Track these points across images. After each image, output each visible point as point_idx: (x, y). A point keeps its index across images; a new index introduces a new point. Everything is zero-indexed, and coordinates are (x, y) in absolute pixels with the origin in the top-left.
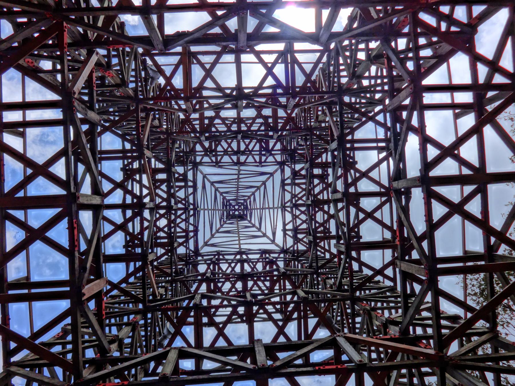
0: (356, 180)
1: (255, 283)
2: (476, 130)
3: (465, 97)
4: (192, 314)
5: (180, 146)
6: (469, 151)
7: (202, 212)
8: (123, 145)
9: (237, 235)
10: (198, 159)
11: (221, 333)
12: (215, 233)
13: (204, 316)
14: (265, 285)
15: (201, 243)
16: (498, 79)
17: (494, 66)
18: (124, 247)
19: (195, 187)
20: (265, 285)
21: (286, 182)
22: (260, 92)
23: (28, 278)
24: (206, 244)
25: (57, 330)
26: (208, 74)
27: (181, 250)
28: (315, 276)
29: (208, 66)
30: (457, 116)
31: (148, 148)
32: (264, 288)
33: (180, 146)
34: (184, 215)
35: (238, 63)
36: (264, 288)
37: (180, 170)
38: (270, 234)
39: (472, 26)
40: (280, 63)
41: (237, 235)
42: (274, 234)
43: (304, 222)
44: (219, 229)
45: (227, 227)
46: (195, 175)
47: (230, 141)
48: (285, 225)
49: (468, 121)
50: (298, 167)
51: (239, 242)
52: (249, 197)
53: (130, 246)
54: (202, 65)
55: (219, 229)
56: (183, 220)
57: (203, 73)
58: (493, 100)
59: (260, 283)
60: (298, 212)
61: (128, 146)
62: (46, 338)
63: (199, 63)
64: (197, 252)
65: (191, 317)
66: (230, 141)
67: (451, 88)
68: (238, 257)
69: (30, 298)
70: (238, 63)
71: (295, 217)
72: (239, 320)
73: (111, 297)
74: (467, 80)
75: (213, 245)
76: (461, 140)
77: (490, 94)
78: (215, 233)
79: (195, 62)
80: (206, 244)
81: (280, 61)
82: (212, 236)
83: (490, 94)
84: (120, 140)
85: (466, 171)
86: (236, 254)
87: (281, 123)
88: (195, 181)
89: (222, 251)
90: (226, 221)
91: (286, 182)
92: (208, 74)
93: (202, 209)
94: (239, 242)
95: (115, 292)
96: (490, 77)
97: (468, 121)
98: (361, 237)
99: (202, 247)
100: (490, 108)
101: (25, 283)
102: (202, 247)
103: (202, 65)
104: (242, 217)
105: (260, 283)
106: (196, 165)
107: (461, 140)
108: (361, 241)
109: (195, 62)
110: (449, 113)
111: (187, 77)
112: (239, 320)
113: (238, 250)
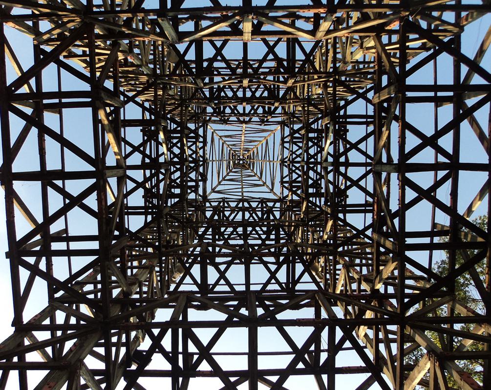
0: (146, 180)
1: (254, 229)
2: (49, 220)
3: (56, 246)
4: (297, 70)
5: (193, 107)
6: (56, 202)
7: (210, 163)
8: (345, 216)
9: (240, 183)
10: (278, 205)
11: (271, 49)
12: (222, 181)
13: (170, 352)
14: (262, 230)
15: (209, 190)
16: (31, 260)
17: (35, 271)
18: (348, 131)
19: (205, 142)
20: (262, 230)
21: (285, 140)
22: (230, 259)
23: (437, 106)
24: (213, 191)
25: (413, 62)
26: (273, 275)
27: (192, 196)
28: (158, 71)
29: (273, 281)
30: (66, 231)
31: (327, 213)
32: (260, 232)
33: (193, 107)
34: (293, 157)
35: (248, 283)
36: (260, 232)
37: (192, 126)
38: (269, 183)
39: (54, 304)
40: (211, 285)
41: (240, 183)
42: (273, 184)
43: (299, 176)
44: (225, 177)
45: (232, 175)
46: (205, 132)
47: (270, 287)
48: (282, 178)
49: (56, 227)
50: (296, 127)
51: (242, 190)
52: (231, 171)
53: (343, 131)
54: (278, 282)
55: (225, 177)
56: (294, 153)
57: (277, 275)
58: (36, 244)
59: (258, 229)
60: (194, 156)
61: (341, 216)
62: (424, 54)
63: (280, 284)
64: (205, 197)
65: (297, 67)
66: (270, 287)
67: (69, 253)
68: (240, 205)
69: (436, 88)
70: (248, 283)
71: (291, 172)
72: (239, 238)
73: (363, 88)
74: (55, 260)
75: (219, 192)
76: (62, 212)
77: (38, 248)
78: (222, 181)
79: (284, 285)
80: (213, 191)
81: (211, 286)
82: (219, 183)
83: (38, 248)
84: (348, 220)
85: (59, 183)
86: (239, 201)
87: (209, 235)
88: (205, 137)
89: (227, 198)
90: (231, 170)
91: (285, 140)
92: (273, 275)
93: (210, 161)
94: (242, 190)
95: (361, 91)
96: (38, 262)
97: (56, 227)
98: (141, 131)
99: (210, 193)
100: (38, 237)
101: (439, 102)
102: (210, 193)
103: (278, 282)
104: (243, 167)
105: (258, 229)
106: (205, 123)
107: (62, 212)
108: (141, 128)
109: (284, 285)
110: (72, 233)
111: (291, 272)
112: (239, 238)
113: (241, 197)
